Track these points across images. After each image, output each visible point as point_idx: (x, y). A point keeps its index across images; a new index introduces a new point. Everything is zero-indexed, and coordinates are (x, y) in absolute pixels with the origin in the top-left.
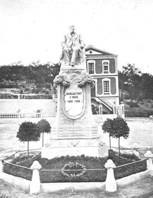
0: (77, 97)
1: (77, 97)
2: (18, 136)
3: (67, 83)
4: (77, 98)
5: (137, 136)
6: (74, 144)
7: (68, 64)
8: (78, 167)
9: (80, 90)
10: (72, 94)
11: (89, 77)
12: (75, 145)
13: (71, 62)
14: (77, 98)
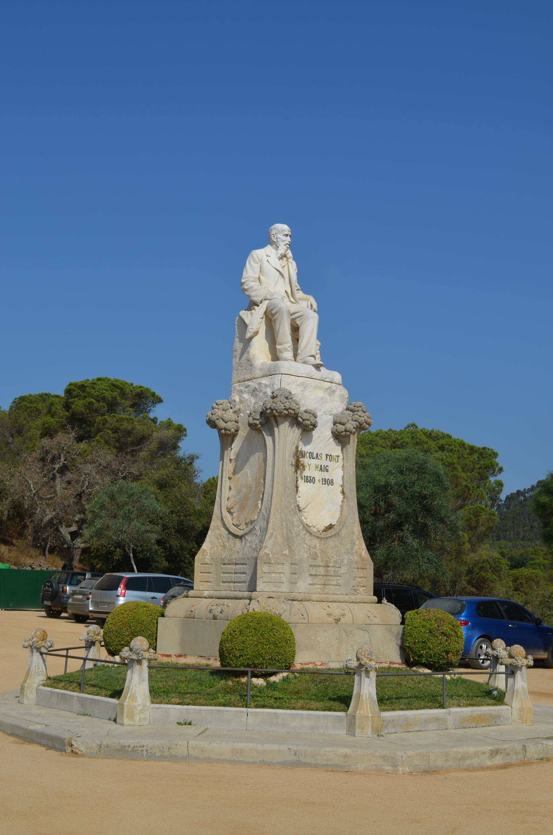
4: (327, 471)
9: (336, 450)
10: (315, 456)
14: (327, 471)
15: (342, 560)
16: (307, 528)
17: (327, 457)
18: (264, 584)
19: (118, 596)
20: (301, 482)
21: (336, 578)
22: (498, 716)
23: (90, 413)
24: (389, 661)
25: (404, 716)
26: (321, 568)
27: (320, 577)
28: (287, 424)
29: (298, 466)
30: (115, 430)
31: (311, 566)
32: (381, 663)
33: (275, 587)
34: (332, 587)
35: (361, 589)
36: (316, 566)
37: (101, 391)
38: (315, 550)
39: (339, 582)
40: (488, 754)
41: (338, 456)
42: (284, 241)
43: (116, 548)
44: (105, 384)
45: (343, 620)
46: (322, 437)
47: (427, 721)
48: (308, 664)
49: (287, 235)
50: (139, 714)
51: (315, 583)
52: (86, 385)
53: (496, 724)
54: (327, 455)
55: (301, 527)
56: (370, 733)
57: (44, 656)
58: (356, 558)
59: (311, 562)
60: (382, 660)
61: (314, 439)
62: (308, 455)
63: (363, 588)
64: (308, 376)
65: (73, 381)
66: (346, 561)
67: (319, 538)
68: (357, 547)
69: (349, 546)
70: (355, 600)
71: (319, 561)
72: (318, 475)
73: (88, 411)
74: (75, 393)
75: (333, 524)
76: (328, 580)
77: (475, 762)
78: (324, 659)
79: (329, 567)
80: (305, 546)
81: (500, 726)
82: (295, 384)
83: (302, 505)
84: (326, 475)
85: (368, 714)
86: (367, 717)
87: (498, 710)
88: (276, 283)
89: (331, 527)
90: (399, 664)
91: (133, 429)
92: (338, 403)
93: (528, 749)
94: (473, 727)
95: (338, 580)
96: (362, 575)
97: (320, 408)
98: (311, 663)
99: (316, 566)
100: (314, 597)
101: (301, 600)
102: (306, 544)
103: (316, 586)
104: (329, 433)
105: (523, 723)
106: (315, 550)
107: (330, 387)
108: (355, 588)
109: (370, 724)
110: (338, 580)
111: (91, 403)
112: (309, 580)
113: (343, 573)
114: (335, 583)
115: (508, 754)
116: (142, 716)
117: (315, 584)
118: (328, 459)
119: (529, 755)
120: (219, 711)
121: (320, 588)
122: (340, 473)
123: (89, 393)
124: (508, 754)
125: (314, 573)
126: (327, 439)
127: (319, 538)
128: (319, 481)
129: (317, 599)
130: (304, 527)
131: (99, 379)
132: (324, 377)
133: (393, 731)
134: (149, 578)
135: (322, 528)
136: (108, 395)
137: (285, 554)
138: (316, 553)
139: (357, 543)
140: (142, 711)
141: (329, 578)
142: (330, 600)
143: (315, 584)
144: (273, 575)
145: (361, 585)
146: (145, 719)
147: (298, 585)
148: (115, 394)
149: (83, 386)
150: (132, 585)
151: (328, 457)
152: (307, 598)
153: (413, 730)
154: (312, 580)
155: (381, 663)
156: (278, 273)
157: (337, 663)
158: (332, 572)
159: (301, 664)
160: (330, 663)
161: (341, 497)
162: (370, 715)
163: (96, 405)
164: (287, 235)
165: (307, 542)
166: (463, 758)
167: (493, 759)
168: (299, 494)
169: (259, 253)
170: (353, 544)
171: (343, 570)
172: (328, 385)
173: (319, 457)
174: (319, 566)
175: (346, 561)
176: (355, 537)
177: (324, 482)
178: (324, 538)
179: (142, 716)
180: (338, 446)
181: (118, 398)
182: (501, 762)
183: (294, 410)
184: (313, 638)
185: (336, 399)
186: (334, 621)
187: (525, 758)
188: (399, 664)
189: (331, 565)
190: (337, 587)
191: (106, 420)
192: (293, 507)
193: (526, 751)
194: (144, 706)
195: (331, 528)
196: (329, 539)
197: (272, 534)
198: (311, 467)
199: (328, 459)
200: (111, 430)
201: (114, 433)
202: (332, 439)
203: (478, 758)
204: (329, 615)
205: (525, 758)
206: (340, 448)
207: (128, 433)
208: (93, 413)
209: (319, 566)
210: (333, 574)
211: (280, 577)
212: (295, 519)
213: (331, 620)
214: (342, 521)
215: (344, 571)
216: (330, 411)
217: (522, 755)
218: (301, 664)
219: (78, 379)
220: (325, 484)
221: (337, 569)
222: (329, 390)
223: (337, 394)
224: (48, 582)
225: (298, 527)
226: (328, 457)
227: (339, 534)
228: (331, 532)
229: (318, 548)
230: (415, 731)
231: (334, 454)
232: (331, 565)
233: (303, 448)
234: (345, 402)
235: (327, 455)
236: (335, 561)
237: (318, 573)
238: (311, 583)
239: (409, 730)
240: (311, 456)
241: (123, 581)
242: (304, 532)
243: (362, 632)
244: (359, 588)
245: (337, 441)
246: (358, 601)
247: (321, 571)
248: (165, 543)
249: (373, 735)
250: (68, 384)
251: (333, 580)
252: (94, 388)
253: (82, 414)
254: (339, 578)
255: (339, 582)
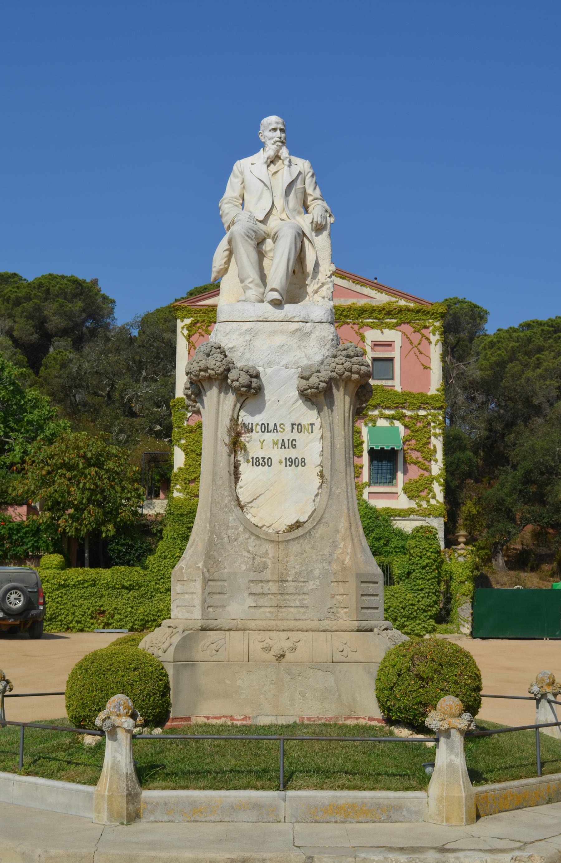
0: (293, 445)
1: (293, 445)
2: (96, 785)
3: (251, 376)
4: (294, 447)
5: (325, 552)
6: (276, 650)
7: (253, 292)
8: (22, 405)
9: (309, 416)
10: (271, 427)
11: (348, 356)
12: (283, 656)
13: (269, 287)
14: (294, 447)
15: (311, 571)
16: (254, 531)
17: (293, 428)
18: (179, 608)
20: (244, 468)
21: (300, 597)
22: (397, 808)
24: (368, 715)
25: (187, 797)
26: (271, 584)
27: (270, 596)
28: (215, 390)
29: (236, 445)
32: (357, 718)
33: (188, 612)
34: (292, 610)
35: (342, 611)
36: (261, 581)
39: (306, 602)
41: (312, 425)
42: (271, 138)
46: (282, 401)
47: (235, 808)
48: (219, 718)
49: (275, 130)
51: (260, 604)
53: (389, 820)
54: (293, 425)
55: (241, 529)
56: (105, 819)
57: (553, 704)
58: (335, 567)
60: (361, 714)
61: (267, 405)
62: (259, 428)
63: (345, 610)
64: (261, 319)
66: (317, 573)
67: (272, 541)
69: (327, 551)
70: (327, 627)
71: (268, 574)
76: (285, 600)
78: (248, 711)
79: (287, 581)
80: (245, 554)
82: (238, 333)
83: (244, 499)
84: (292, 453)
85: (104, 792)
86: (103, 796)
87: (395, 798)
89: (298, 525)
90: (378, 720)
92: (316, 349)
94: (336, 822)
95: (303, 599)
96: (342, 591)
97: (277, 360)
98: (224, 716)
99: (261, 581)
102: (249, 552)
103: (262, 610)
105: (442, 822)
107: (297, 330)
108: (334, 610)
109: (106, 806)
110: (303, 599)
112: (250, 601)
113: (312, 590)
114: (298, 603)
117: (261, 607)
118: (295, 430)
121: (269, 612)
127: (272, 541)
128: (280, 462)
129: (258, 628)
130: (245, 528)
132: (290, 316)
133: (166, 818)
135: (284, 528)
137: (199, 567)
141: (287, 597)
143: (261, 607)
144: (187, 596)
145: (342, 605)
147: (228, 608)
151: (295, 427)
152: (240, 626)
153: (207, 819)
155: (357, 718)
156: (262, 184)
157: (274, 718)
158: (292, 588)
159: (208, 718)
162: (106, 793)
164: (275, 130)
165: (250, 548)
168: (240, 483)
169: (243, 165)
170: (334, 545)
171: (311, 585)
172: (295, 326)
173: (279, 429)
175: (317, 573)
177: (288, 463)
180: (313, 410)
183: (213, 369)
184: (228, 682)
185: (312, 345)
186: (274, 659)
188: (378, 720)
192: (226, 502)
195: (298, 527)
196: (292, 543)
197: (194, 540)
199: (295, 430)
202: (300, 401)
204: (267, 649)
206: (315, 412)
210: (293, 592)
211: (193, 599)
212: (231, 518)
213: (269, 656)
214: (318, 517)
215: (315, 587)
216: (297, 362)
218: (208, 718)
220: (290, 466)
221: (301, 584)
222: (298, 334)
225: (236, 528)
226: (295, 427)
228: (299, 532)
229: (270, 556)
230: (210, 821)
231: (305, 422)
233: (245, 418)
235: (293, 425)
236: (296, 573)
238: (254, 604)
239: (198, 819)
240: (265, 428)
243: (320, 673)
244: (340, 610)
245: (309, 403)
246: (334, 629)
249: (111, 821)
251: (295, 600)
254: (306, 597)
255: (306, 602)
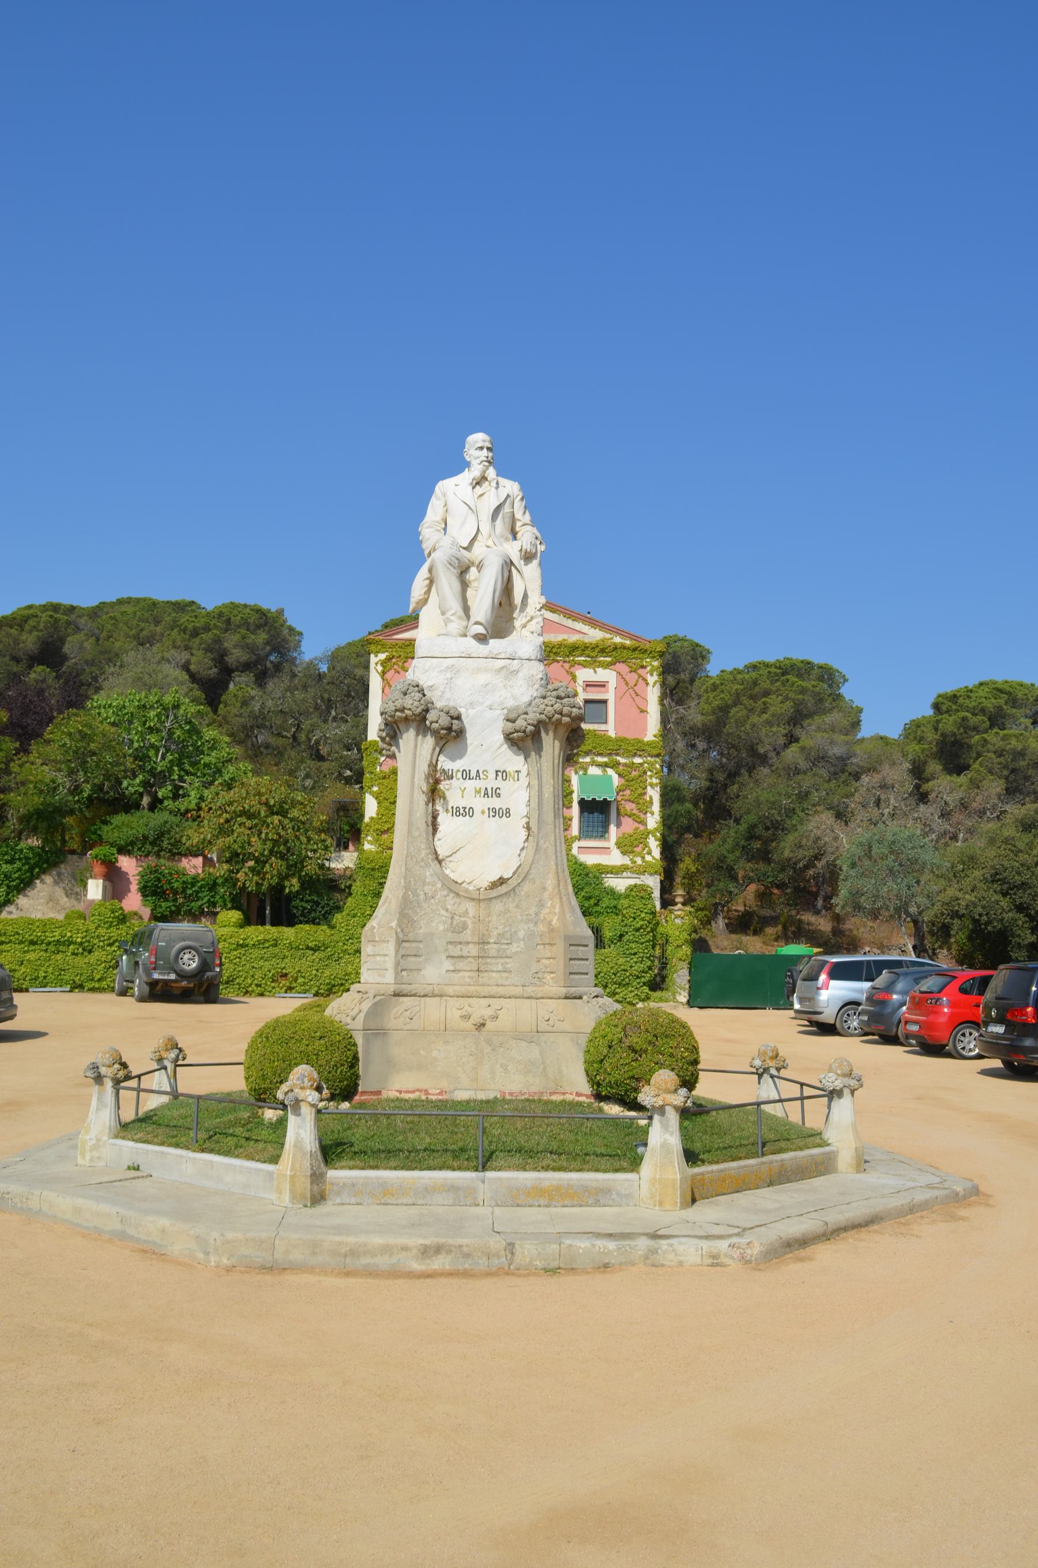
4: (499, 796)
9: (515, 762)
10: (473, 774)
14: (499, 796)
15: (515, 932)
16: (453, 888)
19: (818, 989)
20: (443, 819)
21: (502, 961)
23: (966, 733)
25: (377, 1178)
26: (471, 946)
28: (412, 732)
29: (434, 793)
30: (1000, 753)
31: (451, 943)
32: (564, 1094)
34: (494, 974)
35: (549, 977)
36: (460, 943)
37: (979, 700)
38: (463, 919)
40: (415, 1251)
41: (518, 772)
43: (952, 918)
44: (986, 689)
45: (490, 1025)
47: (429, 1190)
48: (413, 1092)
49: (481, 448)
50: (91, 1151)
51: (458, 968)
52: (958, 694)
53: (597, 1203)
55: (439, 885)
58: (542, 928)
59: (450, 937)
62: (459, 775)
65: (941, 692)
66: (521, 934)
67: (473, 899)
68: (546, 911)
69: (533, 910)
70: (532, 994)
71: (467, 935)
72: (480, 804)
73: (962, 730)
74: (944, 708)
75: (505, 877)
77: (383, 1262)
78: (444, 1085)
80: (444, 913)
81: (607, 1208)
83: (442, 853)
84: (496, 803)
86: (285, 1176)
87: (604, 1180)
88: (464, 523)
89: (502, 881)
90: (587, 1096)
91: (1025, 749)
93: (518, 1249)
94: (539, 1206)
96: (549, 955)
98: (418, 1090)
99: (460, 943)
100: (450, 990)
101: (425, 996)
102: (447, 910)
103: (461, 974)
104: (501, 737)
106: (463, 919)
108: (540, 975)
111: (964, 719)
112: (448, 965)
113: (516, 953)
114: (500, 968)
115: (468, 1256)
116: (96, 1154)
119: (518, 1259)
120: (163, 1153)
122: (523, 796)
123: (961, 706)
124: (468, 1256)
125: (458, 953)
126: (496, 747)
127: (473, 899)
128: (483, 812)
131: (981, 684)
132: (495, 652)
133: (353, 1201)
134: (868, 962)
135: (486, 884)
136: (990, 704)
138: (465, 923)
139: (549, 904)
140: (96, 1147)
141: (489, 960)
142: (483, 994)
144: (378, 958)
146: (99, 1158)
148: (1001, 702)
149: (955, 696)
150: (840, 972)
152: (436, 992)
153: (399, 1201)
154: (453, 965)
155: (564, 1094)
157: (473, 1093)
160: (457, 1092)
161: (524, 833)
162: (289, 1173)
163: (974, 720)
164: (481, 448)
165: (449, 907)
166: (353, 1253)
167: (428, 1261)
168: (438, 835)
170: (541, 905)
171: (514, 948)
172: (500, 663)
174: (468, 943)
175: (521, 934)
176: (546, 895)
177: (492, 814)
178: (484, 900)
179: (96, 1154)
181: (1005, 707)
182: (448, 1267)
184: (422, 1053)
186: (474, 1028)
187: (510, 1265)
188: (587, 1096)
189: (492, 941)
190: (505, 975)
191: (985, 740)
193: (513, 1254)
194: (98, 1140)
195: (502, 884)
196: (494, 901)
198: (455, 792)
200: (995, 753)
201: (1000, 756)
202: (506, 746)
203: (391, 1256)
204: (466, 1017)
205: (510, 1265)
207: (1021, 754)
208: (970, 733)
209: (468, 943)
210: (495, 954)
211: (385, 962)
213: (468, 1025)
214: (523, 874)
215: (519, 949)
217: (504, 1259)
219: (948, 688)
221: (505, 946)
222: (504, 671)
223: (520, 674)
224: (789, 971)
225: (434, 885)
226: (500, 774)
227: (515, 893)
228: (503, 889)
231: (511, 769)
232: (492, 941)
234: (537, 686)
237: (465, 954)
238: (452, 968)
240: (466, 775)
241: (827, 968)
242: (445, 892)
243: (523, 1044)
244: (546, 975)
245: (515, 748)
246: (539, 995)
247: (473, 950)
248: (1028, 908)
249: (293, 1203)
250: (935, 696)
252: (969, 697)
253: (954, 735)
254: (509, 960)
